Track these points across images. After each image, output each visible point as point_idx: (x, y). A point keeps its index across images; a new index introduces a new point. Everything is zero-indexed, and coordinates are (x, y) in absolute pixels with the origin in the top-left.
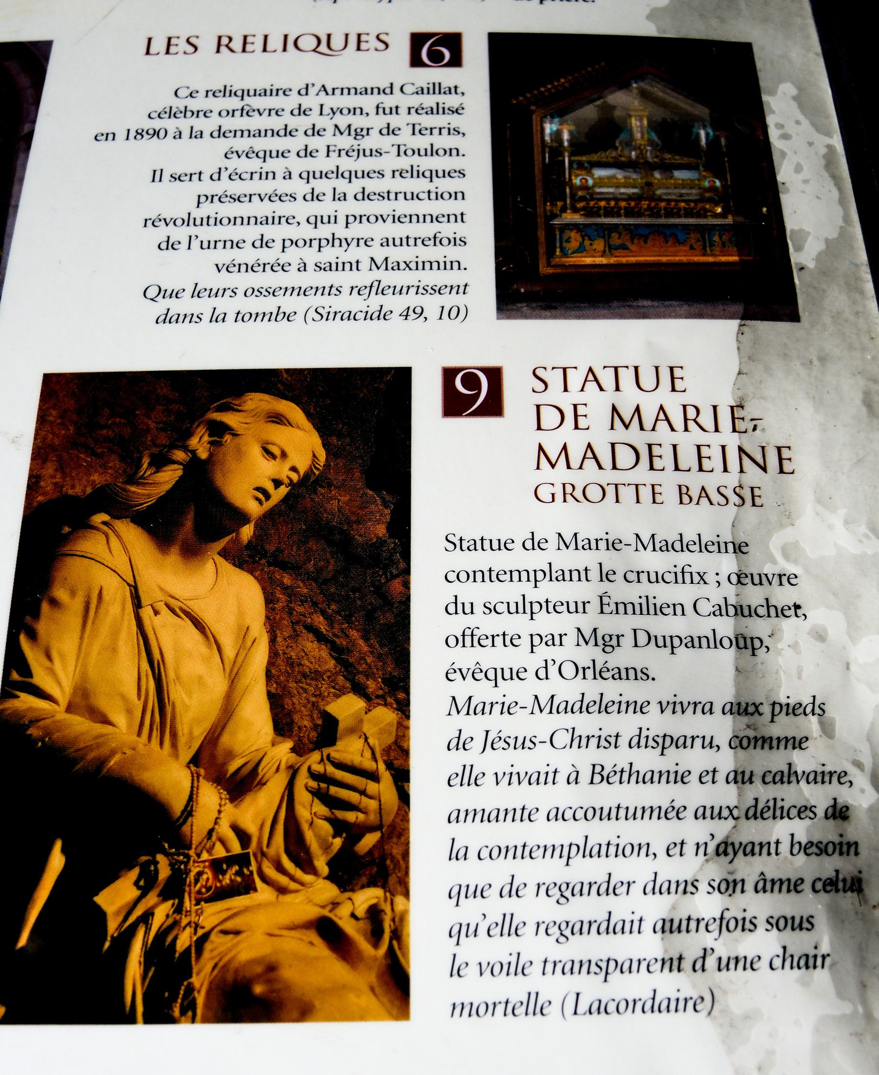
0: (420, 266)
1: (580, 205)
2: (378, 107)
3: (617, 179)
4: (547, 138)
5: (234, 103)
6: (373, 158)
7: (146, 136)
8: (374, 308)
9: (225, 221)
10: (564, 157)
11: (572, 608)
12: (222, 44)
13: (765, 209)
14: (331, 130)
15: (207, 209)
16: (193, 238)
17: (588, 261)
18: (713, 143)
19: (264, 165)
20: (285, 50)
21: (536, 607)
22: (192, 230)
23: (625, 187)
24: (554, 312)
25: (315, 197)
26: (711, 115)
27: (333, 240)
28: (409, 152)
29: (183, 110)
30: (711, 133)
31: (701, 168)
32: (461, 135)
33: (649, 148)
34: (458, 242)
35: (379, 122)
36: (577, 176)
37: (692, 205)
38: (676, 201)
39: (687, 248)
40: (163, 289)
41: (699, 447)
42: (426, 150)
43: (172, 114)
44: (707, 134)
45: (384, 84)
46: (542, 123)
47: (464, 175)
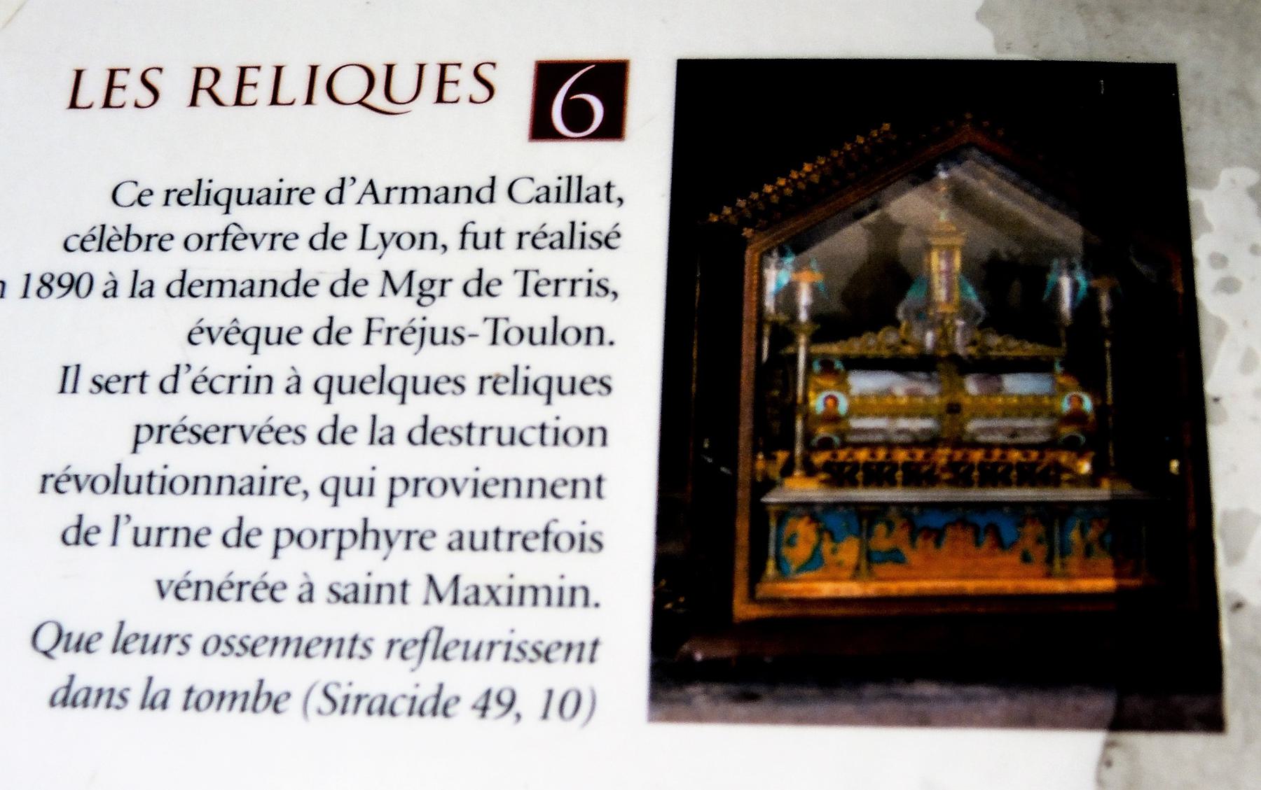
0: (519, 595)
1: (820, 458)
2: (464, 232)
3: (895, 397)
4: (769, 303)
5: (211, 219)
6: (448, 347)
7: (58, 291)
8: (426, 692)
9: (179, 485)
10: (797, 347)
12: (202, 86)
13: (1174, 465)
14: (377, 281)
15: (154, 457)
16: (123, 520)
17: (826, 589)
18: (1086, 305)
19: (254, 360)
20: (309, 101)
22: (121, 504)
23: (908, 415)
24: (754, 708)
25: (339, 435)
26: (1085, 241)
27: (363, 535)
28: (514, 336)
29: (123, 233)
30: (1083, 284)
31: (1058, 369)
32: (610, 296)
33: (960, 323)
34: (588, 543)
35: (460, 265)
36: (819, 390)
37: (1034, 455)
38: (1005, 447)
39: (1015, 559)
40: (66, 631)
42: (544, 329)
43: (103, 241)
44: (1075, 286)
45: (478, 181)
46: (761, 267)
47: (609, 388)
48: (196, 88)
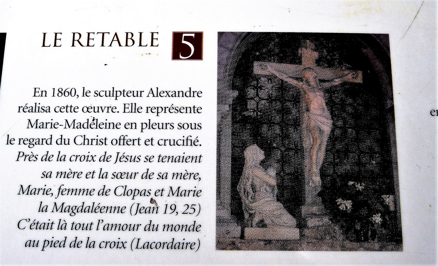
11: (135, 94)
21: (119, 94)
41: (152, 33)
48: (74, 40)
